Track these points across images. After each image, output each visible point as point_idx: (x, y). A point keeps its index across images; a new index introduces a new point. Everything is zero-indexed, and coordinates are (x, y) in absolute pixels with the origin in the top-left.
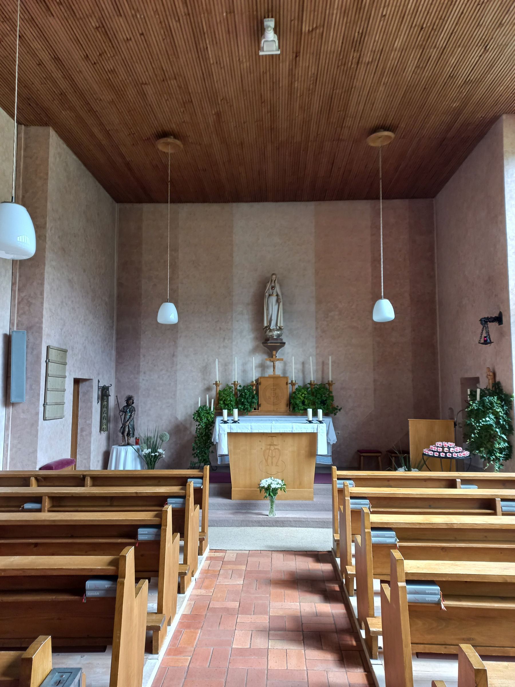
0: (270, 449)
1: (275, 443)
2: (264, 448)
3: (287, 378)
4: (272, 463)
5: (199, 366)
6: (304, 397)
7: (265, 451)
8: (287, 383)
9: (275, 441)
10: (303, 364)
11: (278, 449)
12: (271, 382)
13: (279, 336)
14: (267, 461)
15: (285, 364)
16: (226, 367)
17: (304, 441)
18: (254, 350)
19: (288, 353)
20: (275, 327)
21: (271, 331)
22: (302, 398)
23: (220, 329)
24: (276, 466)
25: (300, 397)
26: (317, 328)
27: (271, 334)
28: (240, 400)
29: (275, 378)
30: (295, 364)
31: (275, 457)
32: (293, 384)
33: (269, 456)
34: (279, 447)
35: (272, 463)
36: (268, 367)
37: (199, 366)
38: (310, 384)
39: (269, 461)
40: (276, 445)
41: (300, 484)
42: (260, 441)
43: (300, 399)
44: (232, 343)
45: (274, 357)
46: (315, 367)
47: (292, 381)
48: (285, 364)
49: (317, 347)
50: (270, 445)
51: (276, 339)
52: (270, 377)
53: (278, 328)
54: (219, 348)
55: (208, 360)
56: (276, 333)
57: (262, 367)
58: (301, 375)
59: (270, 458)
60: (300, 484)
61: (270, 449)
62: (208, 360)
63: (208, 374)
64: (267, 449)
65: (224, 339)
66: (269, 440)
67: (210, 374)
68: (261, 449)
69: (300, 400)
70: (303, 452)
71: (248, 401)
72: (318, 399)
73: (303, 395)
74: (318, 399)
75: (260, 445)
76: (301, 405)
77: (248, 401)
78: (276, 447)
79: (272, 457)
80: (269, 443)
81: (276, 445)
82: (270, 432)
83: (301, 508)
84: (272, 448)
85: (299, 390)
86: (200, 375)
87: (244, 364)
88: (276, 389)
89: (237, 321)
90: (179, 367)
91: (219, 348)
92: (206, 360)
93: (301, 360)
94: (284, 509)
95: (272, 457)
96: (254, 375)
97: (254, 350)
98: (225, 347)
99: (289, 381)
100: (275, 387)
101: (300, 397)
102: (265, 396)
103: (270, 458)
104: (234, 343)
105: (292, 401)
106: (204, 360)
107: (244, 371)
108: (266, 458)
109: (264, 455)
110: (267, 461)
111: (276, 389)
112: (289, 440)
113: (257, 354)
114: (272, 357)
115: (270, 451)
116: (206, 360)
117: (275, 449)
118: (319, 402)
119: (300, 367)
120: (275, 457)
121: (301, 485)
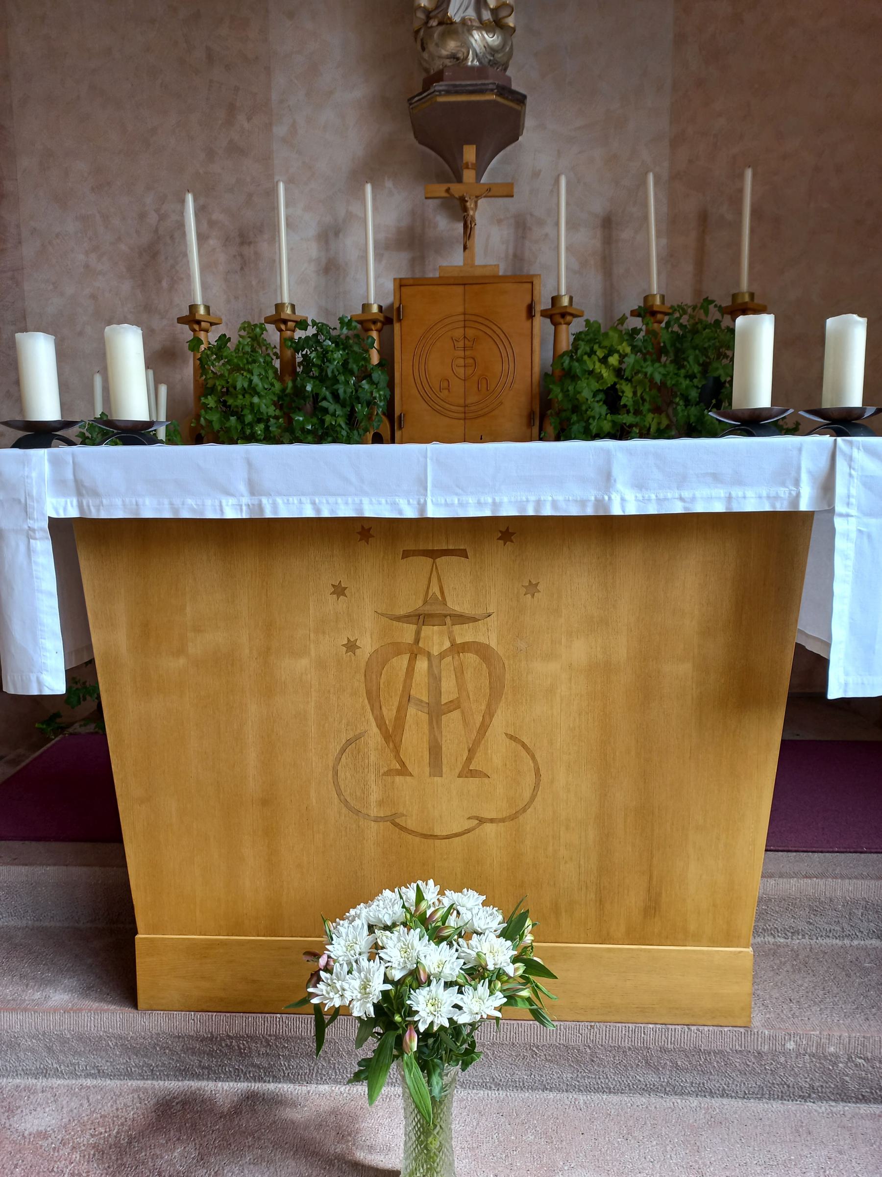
0: (415, 651)
1: (458, 604)
2: (367, 645)
3: (529, 281)
4: (435, 751)
5: (123, 247)
6: (619, 372)
7: (374, 669)
8: (530, 311)
9: (458, 585)
10: (608, 224)
11: (483, 651)
12: (454, 303)
13: (496, 61)
14: (392, 736)
15: (522, 226)
16: (244, 243)
17: (693, 588)
18: (373, 168)
19: (536, 174)
20: (471, 13)
21: (449, 27)
22: (605, 373)
23: (210, 58)
24: (467, 772)
25: (598, 367)
26: (680, 39)
27: (452, 45)
28: (299, 391)
29: (472, 283)
30: (572, 225)
31: (454, 705)
32: (558, 314)
33: (408, 698)
34: (489, 634)
35: (435, 751)
36: (441, 245)
37: (123, 247)
38: (647, 311)
39: (414, 739)
40: (461, 619)
41: (652, 907)
42: (339, 591)
43: (599, 377)
44: (269, 126)
45: (469, 175)
46: (664, 241)
47: (555, 300)
48: (522, 226)
49: (676, 142)
50: (421, 618)
51: (480, 72)
52: (448, 281)
53: (487, 16)
54: (211, 154)
55: (162, 217)
56: (480, 40)
57: (412, 240)
58: (595, 281)
59: (415, 716)
60: (652, 907)
61: (415, 651)
62: (162, 217)
63: (165, 284)
64: (397, 649)
65: (232, 109)
66: (410, 585)
67: (171, 288)
68: (351, 646)
69: (595, 386)
70: (679, 672)
71: (336, 396)
72: (692, 377)
73: (613, 360)
74: (692, 377)
75: (356, 614)
76: (600, 409)
77: (336, 396)
78: (465, 634)
79: (436, 712)
80: (409, 600)
81: (461, 619)
82: (410, 512)
83: (652, 1078)
84: (436, 639)
85: (590, 337)
86: (126, 287)
87: (330, 234)
88: (475, 340)
89: (291, 15)
90: (28, 250)
91: (211, 154)
92: (153, 218)
93: (598, 206)
94: (521, 1074)
95: (436, 712)
96: (373, 285)
97: (373, 168)
98: (235, 150)
99: (544, 303)
100: (470, 333)
101: (598, 367)
102: (424, 364)
103: (415, 716)
104: (280, 130)
105: (557, 393)
106: (142, 216)
107: (332, 269)
108: (389, 713)
109: (373, 697)
110: (392, 736)
111: (475, 340)
112: (574, 581)
113: (389, 184)
114: (459, 179)
115: (422, 665)
116: (153, 218)
117: (458, 649)
118: (694, 394)
119: (590, 239)
120: (454, 705)
121: (654, 919)
